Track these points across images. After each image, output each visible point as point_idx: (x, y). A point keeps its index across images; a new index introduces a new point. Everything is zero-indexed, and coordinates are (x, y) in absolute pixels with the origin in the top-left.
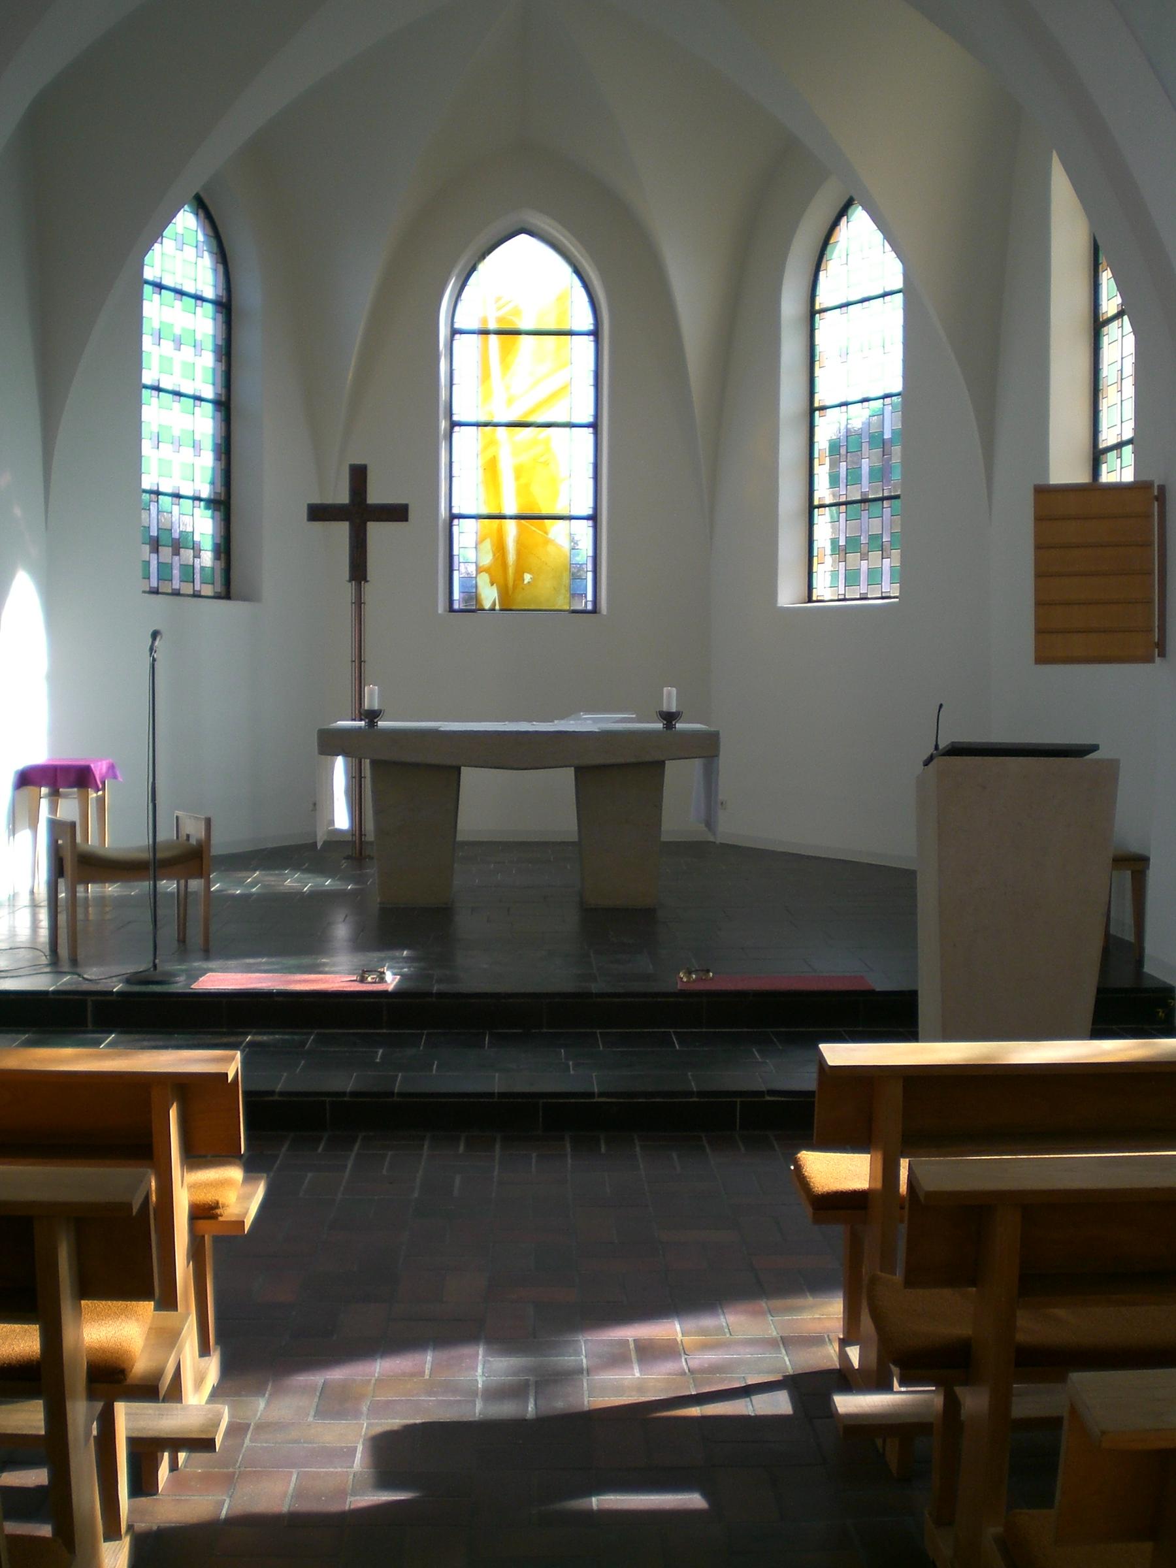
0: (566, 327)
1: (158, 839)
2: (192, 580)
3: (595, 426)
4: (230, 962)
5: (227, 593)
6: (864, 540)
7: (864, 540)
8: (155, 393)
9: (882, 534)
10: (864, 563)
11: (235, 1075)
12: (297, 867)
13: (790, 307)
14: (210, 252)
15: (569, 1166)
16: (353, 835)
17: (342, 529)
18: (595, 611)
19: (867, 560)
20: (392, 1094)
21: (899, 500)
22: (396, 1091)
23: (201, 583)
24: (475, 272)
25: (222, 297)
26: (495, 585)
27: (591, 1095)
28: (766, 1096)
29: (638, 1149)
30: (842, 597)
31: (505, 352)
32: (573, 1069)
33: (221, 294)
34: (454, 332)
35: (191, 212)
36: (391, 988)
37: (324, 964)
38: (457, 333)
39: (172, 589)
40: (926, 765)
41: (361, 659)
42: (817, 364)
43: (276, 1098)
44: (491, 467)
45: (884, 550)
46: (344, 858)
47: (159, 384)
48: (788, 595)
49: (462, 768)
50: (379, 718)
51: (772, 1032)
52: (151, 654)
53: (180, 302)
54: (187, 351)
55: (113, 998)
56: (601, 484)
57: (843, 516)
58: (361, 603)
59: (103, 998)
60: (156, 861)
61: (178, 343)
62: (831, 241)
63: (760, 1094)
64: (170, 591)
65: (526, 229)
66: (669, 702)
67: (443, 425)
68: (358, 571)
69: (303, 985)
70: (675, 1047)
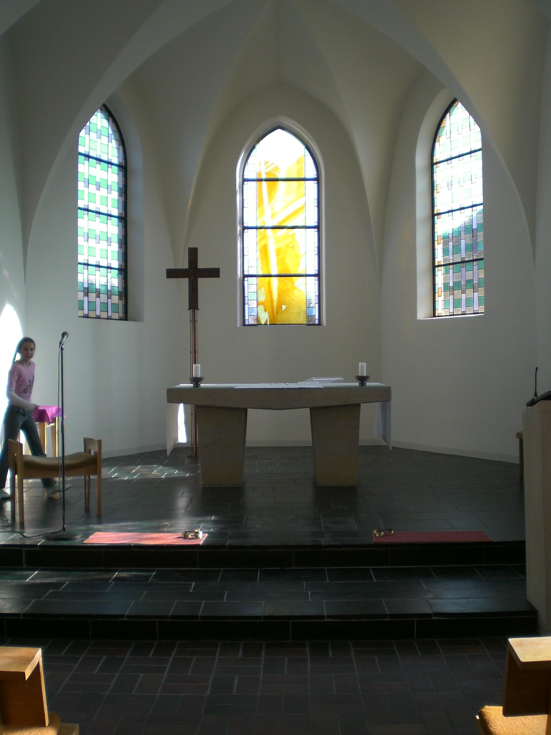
0: (302, 176)
1: (66, 454)
2: (107, 310)
3: (318, 227)
4: (111, 525)
5: (125, 317)
6: (463, 283)
7: (463, 283)
8: (86, 212)
9: (473, 279)
10: (464, 295)
11: (37, 664)
12: (161, 463)
13: (420, 161)
14: (116, 140)
15: (309, 668)
16: (192, 445)
17: (185, 282)
18: (319, 324)
19: (466, 293)
20: (197, 617)
21: (483, 261)
22: (199, 615)
23: (112, 312)
24: (255, 149)
25: (122, 163)
26: (267, 311)
27: (323, 617)
28: (433, 617)
29: (352, 654)
30: (452, 314)
31: (270, 191)
32: (311, 599)
33: (121, 162)
34: (244, 180)
35: (105, 119)
36: (201, 543)
37: (165, 526)
38: (246, 181)
39: (96, 315)
40: (529, 406)
41: (195, 351)
42: (435, 191)
43: (125, 619)
44: (264, 250)
45: (474, 287)
46: (188, 457)
47: (88, 208)
48: (422, 313)
49: (248, 409)
50: (201, 382)
51: (430, 567)
52: (60, 346)
53: (99, 165)
54: (103, 191)
55: (38, 549)
56: (322, 204)
57: (451, 271)
58: (195, 321)
59: (30, 549)
60: (64, 467)
61: (98, 186)
62: (441, 127)
63: (429, 615)
64: (95, 316)
65: (281, 127)
66: (362, 371)
67: (239, 228)
68: (193, 304)
69: (149, 541)
70: (374, 580)
